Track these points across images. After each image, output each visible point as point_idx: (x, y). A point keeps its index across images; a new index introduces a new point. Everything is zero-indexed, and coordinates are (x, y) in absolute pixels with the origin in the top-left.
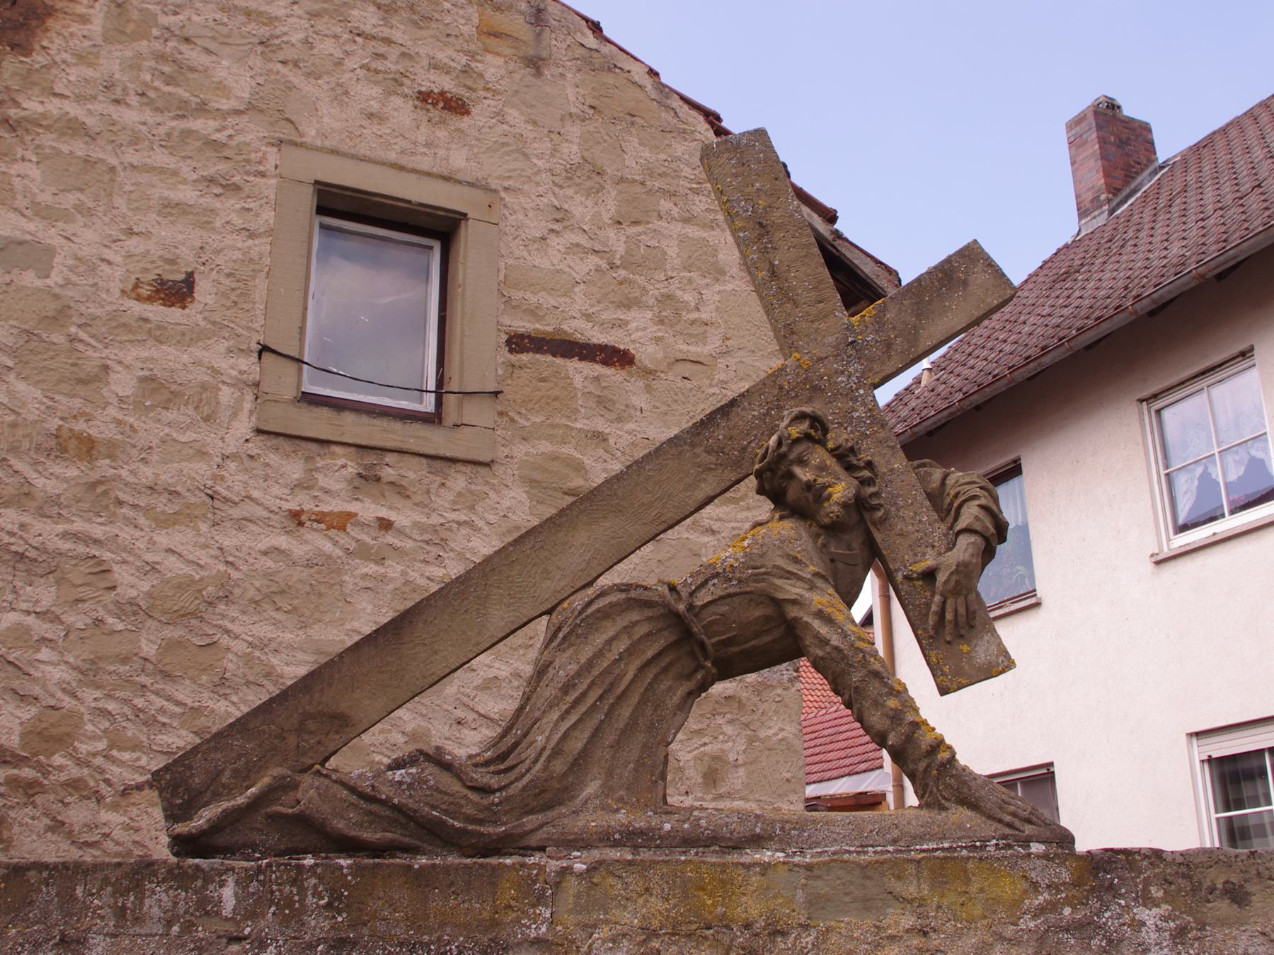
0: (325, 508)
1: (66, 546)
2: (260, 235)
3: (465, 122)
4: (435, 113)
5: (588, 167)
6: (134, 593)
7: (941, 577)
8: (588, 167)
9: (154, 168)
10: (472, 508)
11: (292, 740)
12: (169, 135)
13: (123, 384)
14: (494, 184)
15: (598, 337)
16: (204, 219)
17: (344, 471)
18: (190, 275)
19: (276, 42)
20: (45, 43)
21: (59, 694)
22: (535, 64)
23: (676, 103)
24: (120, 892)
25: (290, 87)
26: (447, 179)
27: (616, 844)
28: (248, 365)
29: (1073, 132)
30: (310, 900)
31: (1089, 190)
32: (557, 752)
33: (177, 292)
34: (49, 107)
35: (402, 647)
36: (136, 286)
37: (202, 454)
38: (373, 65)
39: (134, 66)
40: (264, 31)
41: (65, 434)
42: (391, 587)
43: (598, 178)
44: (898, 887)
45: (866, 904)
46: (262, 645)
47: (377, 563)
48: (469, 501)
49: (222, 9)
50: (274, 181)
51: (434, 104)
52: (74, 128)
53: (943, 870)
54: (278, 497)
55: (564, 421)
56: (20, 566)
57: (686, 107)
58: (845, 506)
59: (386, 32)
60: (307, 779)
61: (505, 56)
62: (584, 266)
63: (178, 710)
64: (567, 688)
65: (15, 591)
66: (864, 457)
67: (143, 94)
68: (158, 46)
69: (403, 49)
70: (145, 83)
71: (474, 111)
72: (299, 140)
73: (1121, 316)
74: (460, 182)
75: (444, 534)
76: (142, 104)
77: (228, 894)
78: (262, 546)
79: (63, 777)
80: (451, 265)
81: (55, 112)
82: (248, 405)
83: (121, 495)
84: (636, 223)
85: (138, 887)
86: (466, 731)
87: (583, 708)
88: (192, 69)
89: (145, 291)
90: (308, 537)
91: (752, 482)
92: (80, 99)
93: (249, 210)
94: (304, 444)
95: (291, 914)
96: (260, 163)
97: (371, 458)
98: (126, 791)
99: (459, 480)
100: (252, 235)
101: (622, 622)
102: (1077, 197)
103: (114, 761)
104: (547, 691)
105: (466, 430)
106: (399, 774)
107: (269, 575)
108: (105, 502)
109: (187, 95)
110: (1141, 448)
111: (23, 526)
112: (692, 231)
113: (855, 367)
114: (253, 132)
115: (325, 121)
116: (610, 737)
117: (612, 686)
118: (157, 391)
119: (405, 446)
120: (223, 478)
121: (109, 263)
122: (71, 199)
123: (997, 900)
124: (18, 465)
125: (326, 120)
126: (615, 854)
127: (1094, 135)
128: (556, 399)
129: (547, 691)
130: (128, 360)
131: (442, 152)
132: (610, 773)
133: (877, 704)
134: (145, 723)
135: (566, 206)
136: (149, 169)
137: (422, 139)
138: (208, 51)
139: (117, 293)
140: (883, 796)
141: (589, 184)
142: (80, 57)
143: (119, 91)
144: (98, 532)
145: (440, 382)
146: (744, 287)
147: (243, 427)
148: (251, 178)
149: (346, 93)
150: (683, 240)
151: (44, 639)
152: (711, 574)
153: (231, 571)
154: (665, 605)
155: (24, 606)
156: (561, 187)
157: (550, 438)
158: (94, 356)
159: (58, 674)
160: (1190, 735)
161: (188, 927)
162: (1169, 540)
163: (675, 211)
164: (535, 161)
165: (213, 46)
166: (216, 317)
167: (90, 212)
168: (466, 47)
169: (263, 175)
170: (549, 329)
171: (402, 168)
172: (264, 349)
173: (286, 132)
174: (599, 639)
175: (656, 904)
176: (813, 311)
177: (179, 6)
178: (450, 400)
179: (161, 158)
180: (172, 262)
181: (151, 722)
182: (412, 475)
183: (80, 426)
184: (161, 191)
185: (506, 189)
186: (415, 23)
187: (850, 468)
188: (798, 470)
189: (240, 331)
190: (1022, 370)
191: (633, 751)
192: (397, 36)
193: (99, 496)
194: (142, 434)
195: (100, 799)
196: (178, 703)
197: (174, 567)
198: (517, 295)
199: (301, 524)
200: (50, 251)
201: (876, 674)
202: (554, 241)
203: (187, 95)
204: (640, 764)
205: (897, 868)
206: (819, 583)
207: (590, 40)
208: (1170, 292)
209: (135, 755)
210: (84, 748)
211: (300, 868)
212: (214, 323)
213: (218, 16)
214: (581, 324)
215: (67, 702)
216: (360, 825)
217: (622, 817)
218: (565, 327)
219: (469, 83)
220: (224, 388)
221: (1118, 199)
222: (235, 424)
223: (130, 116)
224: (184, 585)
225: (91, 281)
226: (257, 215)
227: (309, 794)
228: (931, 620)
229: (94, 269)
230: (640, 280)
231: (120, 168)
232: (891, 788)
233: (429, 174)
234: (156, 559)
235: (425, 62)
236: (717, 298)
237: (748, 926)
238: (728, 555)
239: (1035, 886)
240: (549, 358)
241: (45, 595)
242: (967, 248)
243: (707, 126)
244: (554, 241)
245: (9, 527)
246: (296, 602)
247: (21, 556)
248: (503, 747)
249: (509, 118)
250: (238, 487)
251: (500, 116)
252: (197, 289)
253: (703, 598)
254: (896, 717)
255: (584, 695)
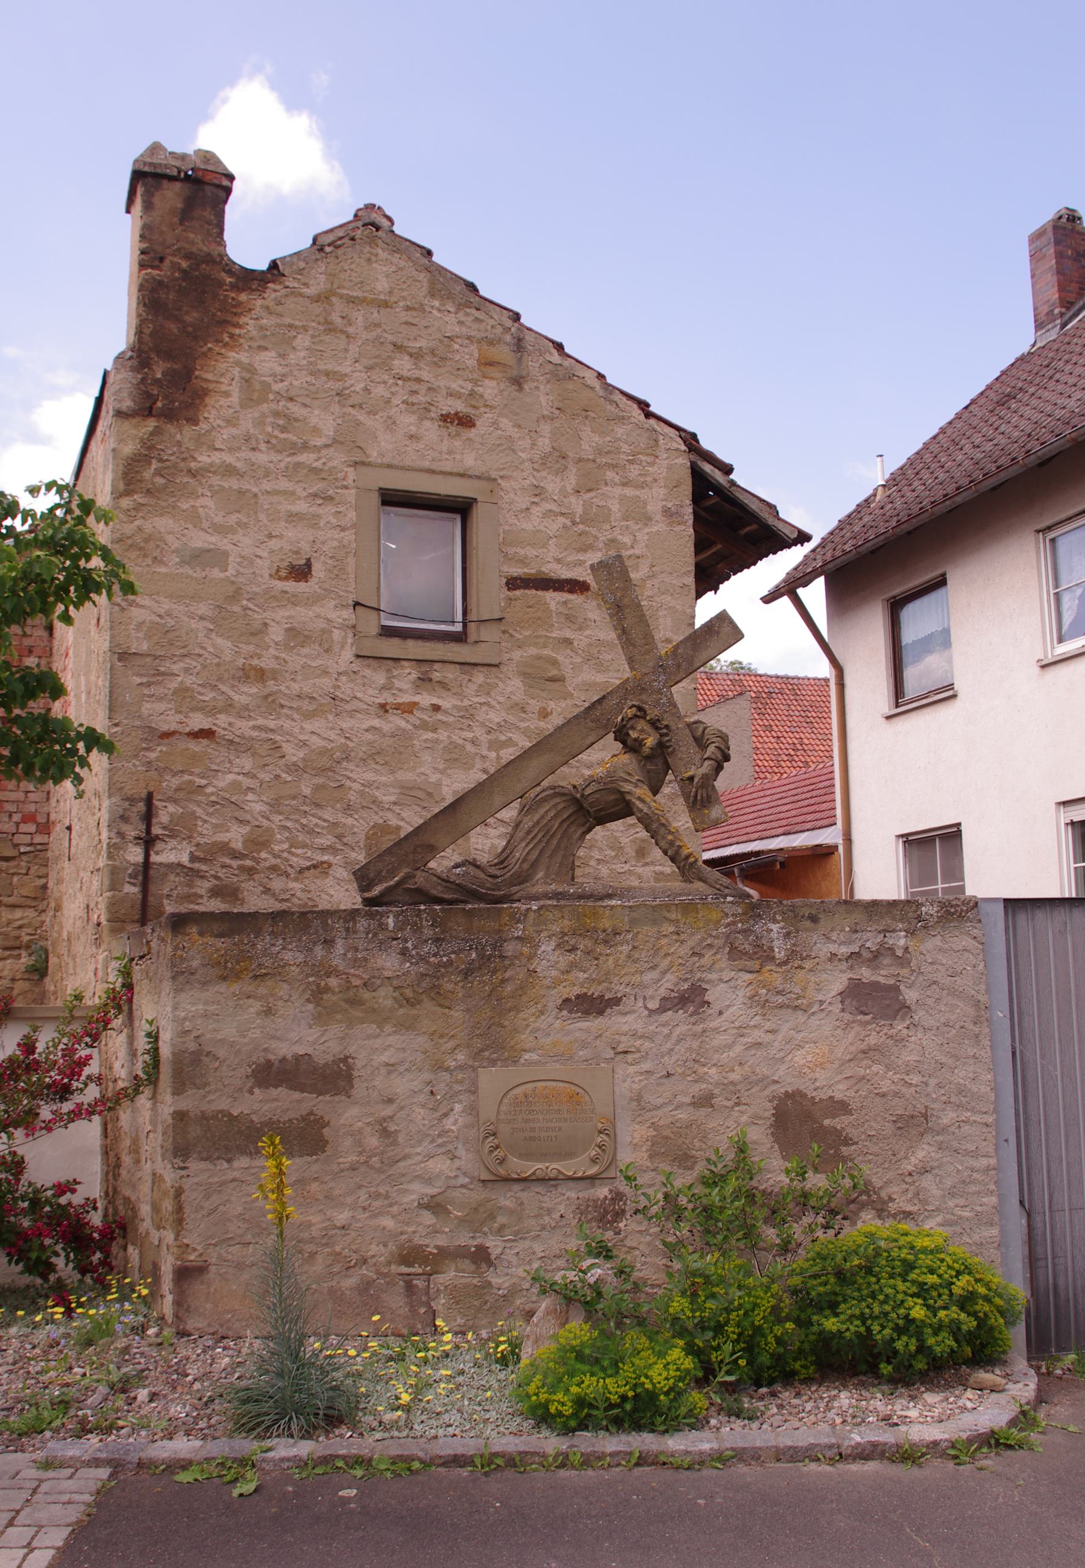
0: (400, 701)
1: (255, 734)
2: (348, 529)
3: (472, 433)
4: (453, 429)
5: (556, 454)
6: (295, 759)
7: (696, 780)
8: (556, 454)
9: (281, 492)
10: (488, 694)
11: (411, 857)
12: (287, 468)
13: (276, 633)
14: (494, 474)
15: (566, 574)
16: (312, 521)
17: (410, 677)
18: (309, 560)
19: (347, 392)
20: (206, 415)
21: (260, 819)
22: (518, 382)
23: (618, 397)
24: (346, 921)
25: (359, 424)
26: (462, 475)
27: (550, 898)
28: (347, 614)
29: (1034, 245)
30: (424, 923)
31: (1045, 303)
32: (524, 860)
33: (301, 572)
34: (214, 458)
35: (455, 815)
36: (278, 571)
37: (326, 673)
38: (410, 400)
39: (260, 423)
40: (339, 385)
41: (247, 667)
42: (442, 746)
43: (563, 462)
44: (668, 915)
45: (655, 922)
46: (369, 785)
47: (432, 732)
48: (486, 689)
49: (311, 374)
50: (353, 491)
51: (452, 423)
52: (229, 471)
53: (688, 908)
54: (372, 696)
55: (544, 633)
56: (232, 747)
57: (624, 399)
58: (652, 749)
59: (417, 374)
60: (419, 873)
61: (497, 379)
62: (555, 526)
63: (326, 824)
64: (528, 832)
65: (230, 762)
66: (665, 723)
67: (268, 442)
68: (273, 406)
69: (429, 385)
70: (269, 434)
71: (478, 423)
72: (367, 460)
73: (1015, 467)
74: (470, 477)
75: (472, 712)
76: (269, 449)
77: (391, 921)
78: (364, 726)
79: (267, 864)
80: (468, 525)
81: (218, 461)
82: (350, 641)
83: (282, 702)
84: (590, 490)
85: (354, 919)
86: (490, 830)
87: (535, 841)
88: (296, 420)
89: (283, 573)
90: (392, 719)
91: (611, 735)
92: (231, 450)
93: (340, 512)
94: (385, 662)
95: (417, 929)
96: (344, 479)
97: (425, 667)
98: (301, 871)
99: (479, 677)
100: (343, 530)
101: (552, 803)
102: (1035, 309)
103: (293, 854)
104: (520, 834)
105: (482, 644)
106: (458, 870)
107: (370, 743)
108: (274, 706)
109: (295, 438)
110: (1035, 571)
111: (230, 724)
112: (629, 492)
113: (662, 678)
114: (337, 459)
115: (383, 445)
116: (548, 853)
117: (548, 831)
118: (297, 636)
119: (446, 658)
120: (339, 687)
121: (261, 557)
122: (233, 518)
123: (710, 920)
124: (224, 688)
125: (383, 444)
126: (550, 902)
127: (1052, 251)
128: (539, 619)
129: (520, 834)
130: (278, 619)
131: (458, 457)
132: (548, 868)
133: (664, 838)
134: (308, 833)
135: (542, 484)
136: (277, 493)
137: (445, 449)
138: (305, 405)
139: (267, 576)
140: (836, 847)
141: (558, 466)
142: (228, 421)
143: (253, 441)
144: (272, 724)
145: (465, 613)
146: (665, 528)
147: (348, 654)
148: (339, 491)
149: (394, 423)
150: (623, 499)
151: (249, 788)
152: (592, 780)
153: (348, 742)
154: (571, 795)
155: (236, 770)
156: (538, 471)
157: (536, 645)
158: (258, 617)
159: (258, 807)
160: (1059, 804)
161: (375, 935)
162: (1053, 648)
163: (617, 479)
164: (520, 454)
165: (307, 401)
166: (326, 586)
167: (245, 526)
168: (470, 377)
169: (346, 487)
170: (533, 571)
171: (433, 472)
172: (357, 604)
173: (358, 456)
174: (542, 811)
175: (566, 922)
176: (643, 650)
177: (284, 375)
178: (472, 627)
179: (284, 484)
180: (297, 553)
181: (311, 832)
182: (451, 676)
183: (255, 662)
184: (286, 507)
185: (501, 477)
186: (436, 364)
187: (657, 728)
188: (631, 732)
189: (342, 593)
190: (941, 506)
191: (558, 858)
192: (425, 375)
193: (271, 703)
194: (291, 663)
195: (288, 876)
196: (325, 821)
197: (316, 742)
198: (511, 551)
199: (387, 711)
200: (226, 554)
201: (663, 825)
202: (535, 510)
203: (295, 438)
204: (561, 863)
205: (667, 907)
206: (640, 784)
207: (556, 358)
208: (1050, 451)
209: (305, 850)
210: (276, 848)
211: (419, 910)
212: (325, 590)
213: (308, 379)
214: (554, 566)
215: (265, 823)
216: (442, 892)
217: (553, 887)
218: (543, 569)
219: (474, 403)
220: (335, 630)
221: (1071, 313)
222: (344, 653)
223: (262, 458)
224: (323, 752)
225: (251, 571)
226: (345, 515)
227: (420, 879)
228: (691, 799)
229: (252, 563)
230: (593, 531)
231: (260, 494)
232: (841, 842)
233: (451, 474)
234: (306, 738)
235: (444, 392)
236: (646, 537)
237: (604, 931)
238: (600, 771)
239: (727, 915)
240: (534, 592)
241: (247, 763)
242: (721, 613)
243: (640, 412)
244: (535, 510)
245: (223, 725)
246: (387, 759)
247: (231, 742)
248: (502, 858)
249: (501, 425)
250: (349, 692)
251: (495, 424)
252: (313, 568)
253: (588, 791)
254: (671, 843)
255: (536, 835)
